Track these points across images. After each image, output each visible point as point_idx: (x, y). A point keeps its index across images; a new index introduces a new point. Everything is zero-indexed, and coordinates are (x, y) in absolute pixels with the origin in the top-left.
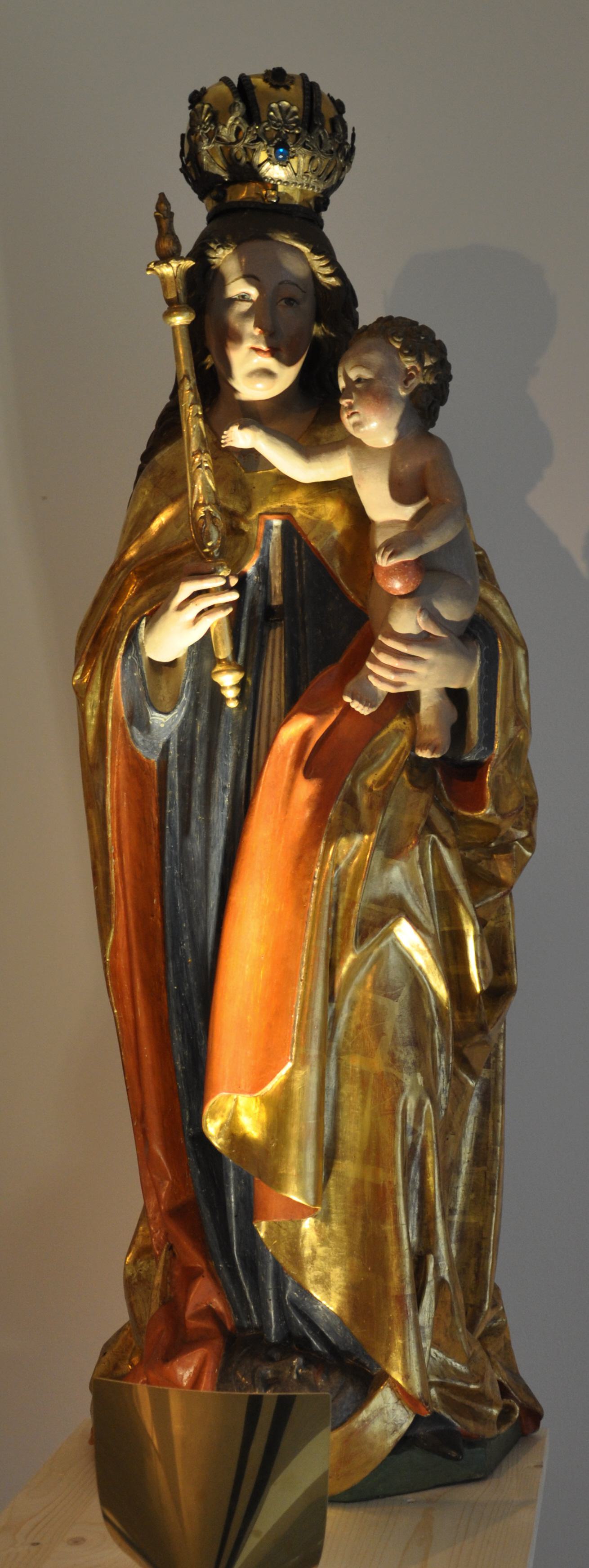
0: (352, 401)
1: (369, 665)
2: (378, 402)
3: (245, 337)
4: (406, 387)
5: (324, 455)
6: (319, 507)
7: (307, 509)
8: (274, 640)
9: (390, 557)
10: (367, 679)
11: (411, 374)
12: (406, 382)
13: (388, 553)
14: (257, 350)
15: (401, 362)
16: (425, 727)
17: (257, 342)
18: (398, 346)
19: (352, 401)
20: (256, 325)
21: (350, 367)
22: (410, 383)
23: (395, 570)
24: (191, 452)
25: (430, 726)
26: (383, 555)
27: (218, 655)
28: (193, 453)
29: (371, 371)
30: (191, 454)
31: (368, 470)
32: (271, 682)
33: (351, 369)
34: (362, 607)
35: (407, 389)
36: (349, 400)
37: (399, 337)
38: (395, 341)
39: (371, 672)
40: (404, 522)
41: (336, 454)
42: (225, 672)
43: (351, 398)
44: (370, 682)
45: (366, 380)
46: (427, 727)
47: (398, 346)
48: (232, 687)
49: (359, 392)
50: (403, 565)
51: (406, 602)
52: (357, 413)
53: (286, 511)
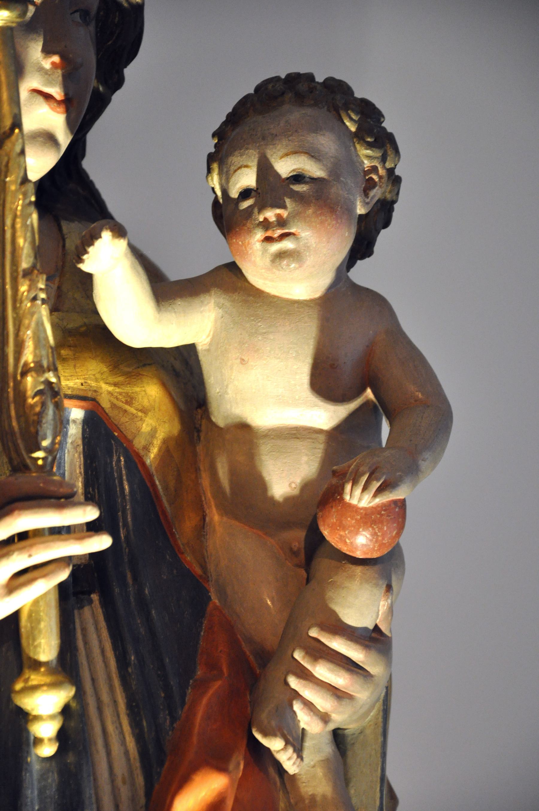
0: (284, 213)
1: (294, 682)
2: (336, 219)
3: (29, 68)
4: (368, 200)
5: (179, 302)
6: (136, 392)
7: (120, 394)
8: (84, 630)
9: (380, 491)
10: (291, 706)
11: (371, 179)
12: (366, 192)
13: (376, 485)
14: (48, 97)
15: (358, 155)
16: (313, 798)
17: (49, 83)
18: (353, 128)
19: (284, 213)
20: (47, 51)
21: (281, 153)
22: (372, 193)
23: (382, 515)
24: (20, 270)
25: (324, 797)
26: (365, 489)
27: (35, 653)
28: (24, 270)
29: (323, 165)
30: (21, 273)
31: (271, 337)
32: (100, 709)
33: (282, 157)
34: (201, 576)
35: (368, 203)
36: (278, 211)
37: (357, 113)
38: (351, 119)
39: (296, 695)
40: (320, 431)
41: (196, 301)
42: (45, 688)
43: (284, 207)
44: (294, 712)
45: (313, 180)
46: (318, 799)
47: (353, 128)
48: (52, 717)
49: (299, 198)
50: (393, 506)
51: (369, 571)
52: (293, 234)
53: (90, 394)
